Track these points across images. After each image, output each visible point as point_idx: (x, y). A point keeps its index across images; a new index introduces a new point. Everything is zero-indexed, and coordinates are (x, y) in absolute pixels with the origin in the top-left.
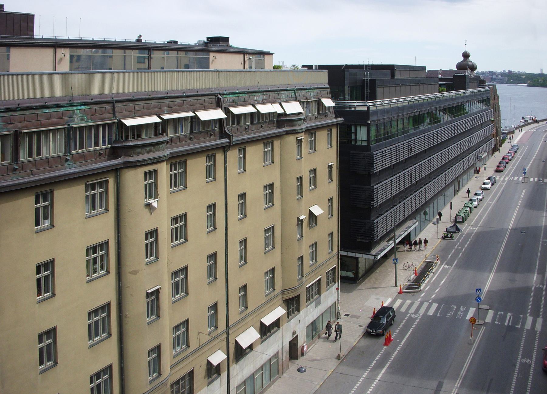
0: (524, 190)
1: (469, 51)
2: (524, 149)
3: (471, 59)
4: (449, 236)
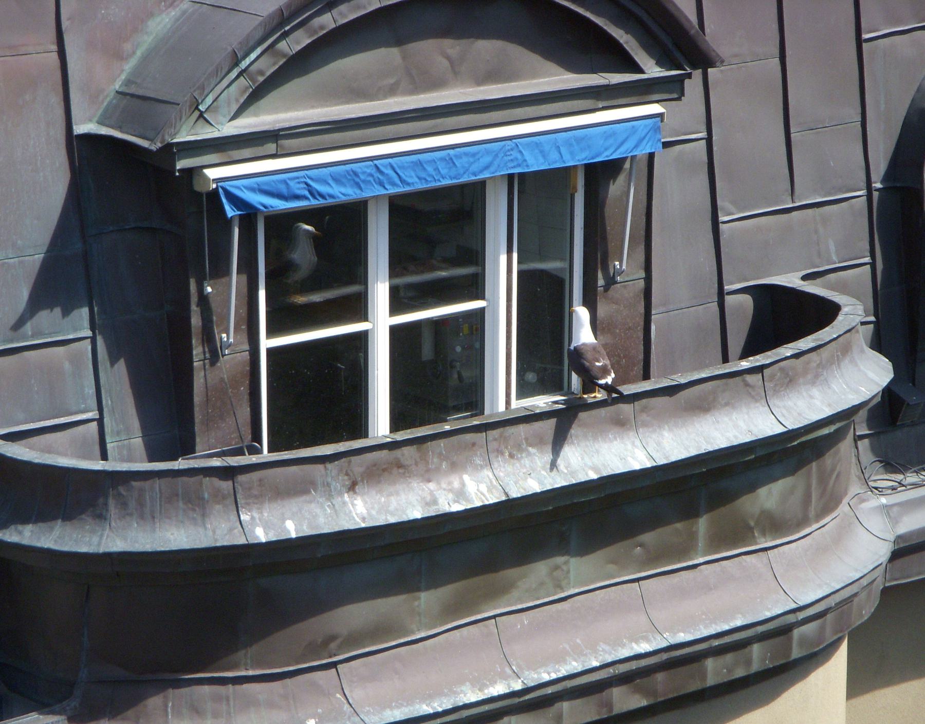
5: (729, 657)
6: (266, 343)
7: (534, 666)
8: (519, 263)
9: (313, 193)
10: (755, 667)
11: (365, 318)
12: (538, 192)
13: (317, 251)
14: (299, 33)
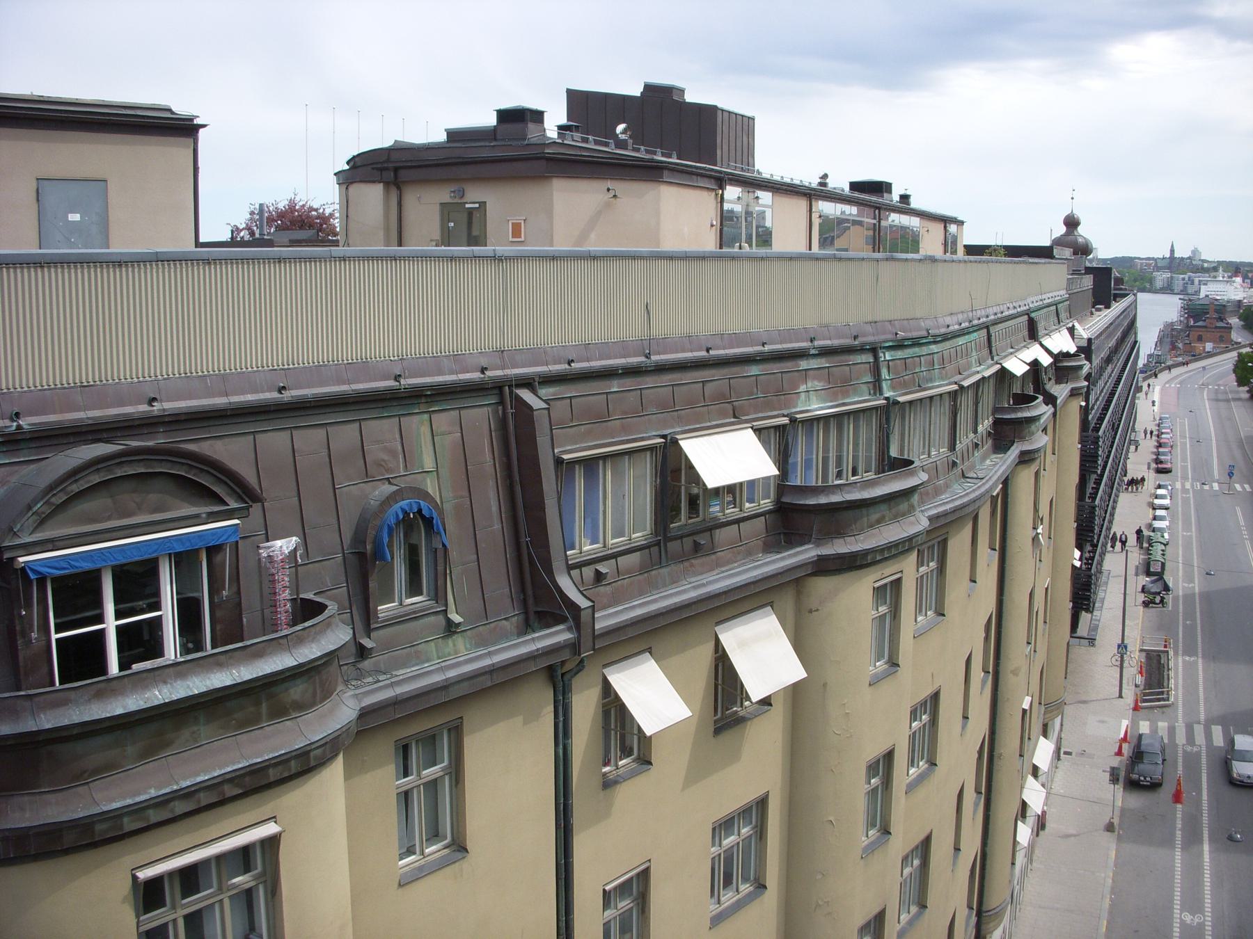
0: (1238, 509)
1: (1078, 213)
2: (1183, 425)
3: (1081, 230)
4: (1158, 599)
5: (280, 768)
6: (55, 636)
7: (185, 779)
8: (55, 617)
9: (72, 567)
10: (293, 771)
11: (160, 609)
12: (184, 560)
13: (77, 593)
14: (61, 494)
